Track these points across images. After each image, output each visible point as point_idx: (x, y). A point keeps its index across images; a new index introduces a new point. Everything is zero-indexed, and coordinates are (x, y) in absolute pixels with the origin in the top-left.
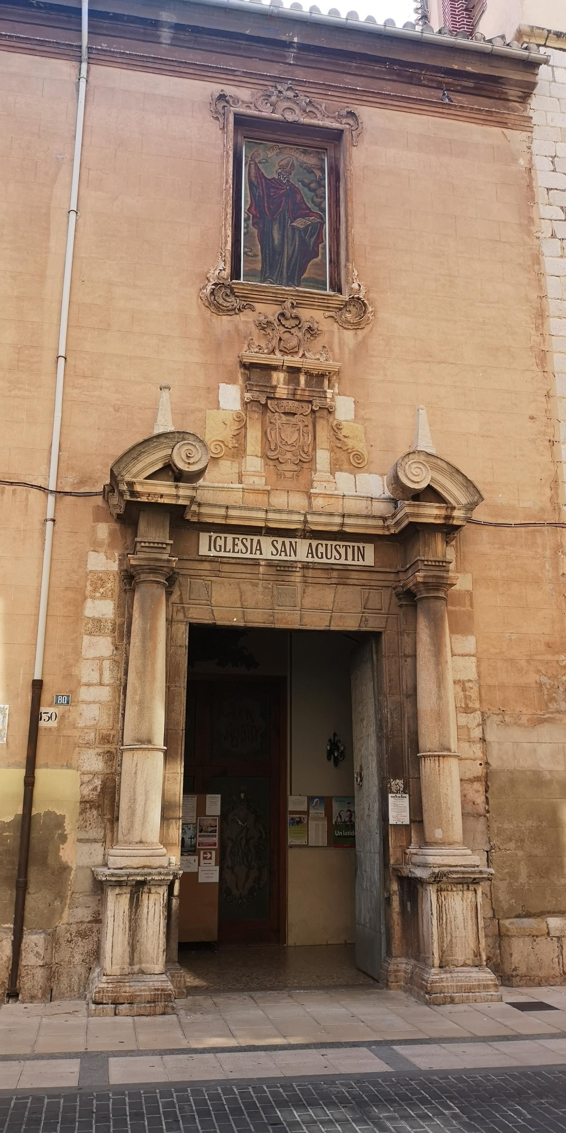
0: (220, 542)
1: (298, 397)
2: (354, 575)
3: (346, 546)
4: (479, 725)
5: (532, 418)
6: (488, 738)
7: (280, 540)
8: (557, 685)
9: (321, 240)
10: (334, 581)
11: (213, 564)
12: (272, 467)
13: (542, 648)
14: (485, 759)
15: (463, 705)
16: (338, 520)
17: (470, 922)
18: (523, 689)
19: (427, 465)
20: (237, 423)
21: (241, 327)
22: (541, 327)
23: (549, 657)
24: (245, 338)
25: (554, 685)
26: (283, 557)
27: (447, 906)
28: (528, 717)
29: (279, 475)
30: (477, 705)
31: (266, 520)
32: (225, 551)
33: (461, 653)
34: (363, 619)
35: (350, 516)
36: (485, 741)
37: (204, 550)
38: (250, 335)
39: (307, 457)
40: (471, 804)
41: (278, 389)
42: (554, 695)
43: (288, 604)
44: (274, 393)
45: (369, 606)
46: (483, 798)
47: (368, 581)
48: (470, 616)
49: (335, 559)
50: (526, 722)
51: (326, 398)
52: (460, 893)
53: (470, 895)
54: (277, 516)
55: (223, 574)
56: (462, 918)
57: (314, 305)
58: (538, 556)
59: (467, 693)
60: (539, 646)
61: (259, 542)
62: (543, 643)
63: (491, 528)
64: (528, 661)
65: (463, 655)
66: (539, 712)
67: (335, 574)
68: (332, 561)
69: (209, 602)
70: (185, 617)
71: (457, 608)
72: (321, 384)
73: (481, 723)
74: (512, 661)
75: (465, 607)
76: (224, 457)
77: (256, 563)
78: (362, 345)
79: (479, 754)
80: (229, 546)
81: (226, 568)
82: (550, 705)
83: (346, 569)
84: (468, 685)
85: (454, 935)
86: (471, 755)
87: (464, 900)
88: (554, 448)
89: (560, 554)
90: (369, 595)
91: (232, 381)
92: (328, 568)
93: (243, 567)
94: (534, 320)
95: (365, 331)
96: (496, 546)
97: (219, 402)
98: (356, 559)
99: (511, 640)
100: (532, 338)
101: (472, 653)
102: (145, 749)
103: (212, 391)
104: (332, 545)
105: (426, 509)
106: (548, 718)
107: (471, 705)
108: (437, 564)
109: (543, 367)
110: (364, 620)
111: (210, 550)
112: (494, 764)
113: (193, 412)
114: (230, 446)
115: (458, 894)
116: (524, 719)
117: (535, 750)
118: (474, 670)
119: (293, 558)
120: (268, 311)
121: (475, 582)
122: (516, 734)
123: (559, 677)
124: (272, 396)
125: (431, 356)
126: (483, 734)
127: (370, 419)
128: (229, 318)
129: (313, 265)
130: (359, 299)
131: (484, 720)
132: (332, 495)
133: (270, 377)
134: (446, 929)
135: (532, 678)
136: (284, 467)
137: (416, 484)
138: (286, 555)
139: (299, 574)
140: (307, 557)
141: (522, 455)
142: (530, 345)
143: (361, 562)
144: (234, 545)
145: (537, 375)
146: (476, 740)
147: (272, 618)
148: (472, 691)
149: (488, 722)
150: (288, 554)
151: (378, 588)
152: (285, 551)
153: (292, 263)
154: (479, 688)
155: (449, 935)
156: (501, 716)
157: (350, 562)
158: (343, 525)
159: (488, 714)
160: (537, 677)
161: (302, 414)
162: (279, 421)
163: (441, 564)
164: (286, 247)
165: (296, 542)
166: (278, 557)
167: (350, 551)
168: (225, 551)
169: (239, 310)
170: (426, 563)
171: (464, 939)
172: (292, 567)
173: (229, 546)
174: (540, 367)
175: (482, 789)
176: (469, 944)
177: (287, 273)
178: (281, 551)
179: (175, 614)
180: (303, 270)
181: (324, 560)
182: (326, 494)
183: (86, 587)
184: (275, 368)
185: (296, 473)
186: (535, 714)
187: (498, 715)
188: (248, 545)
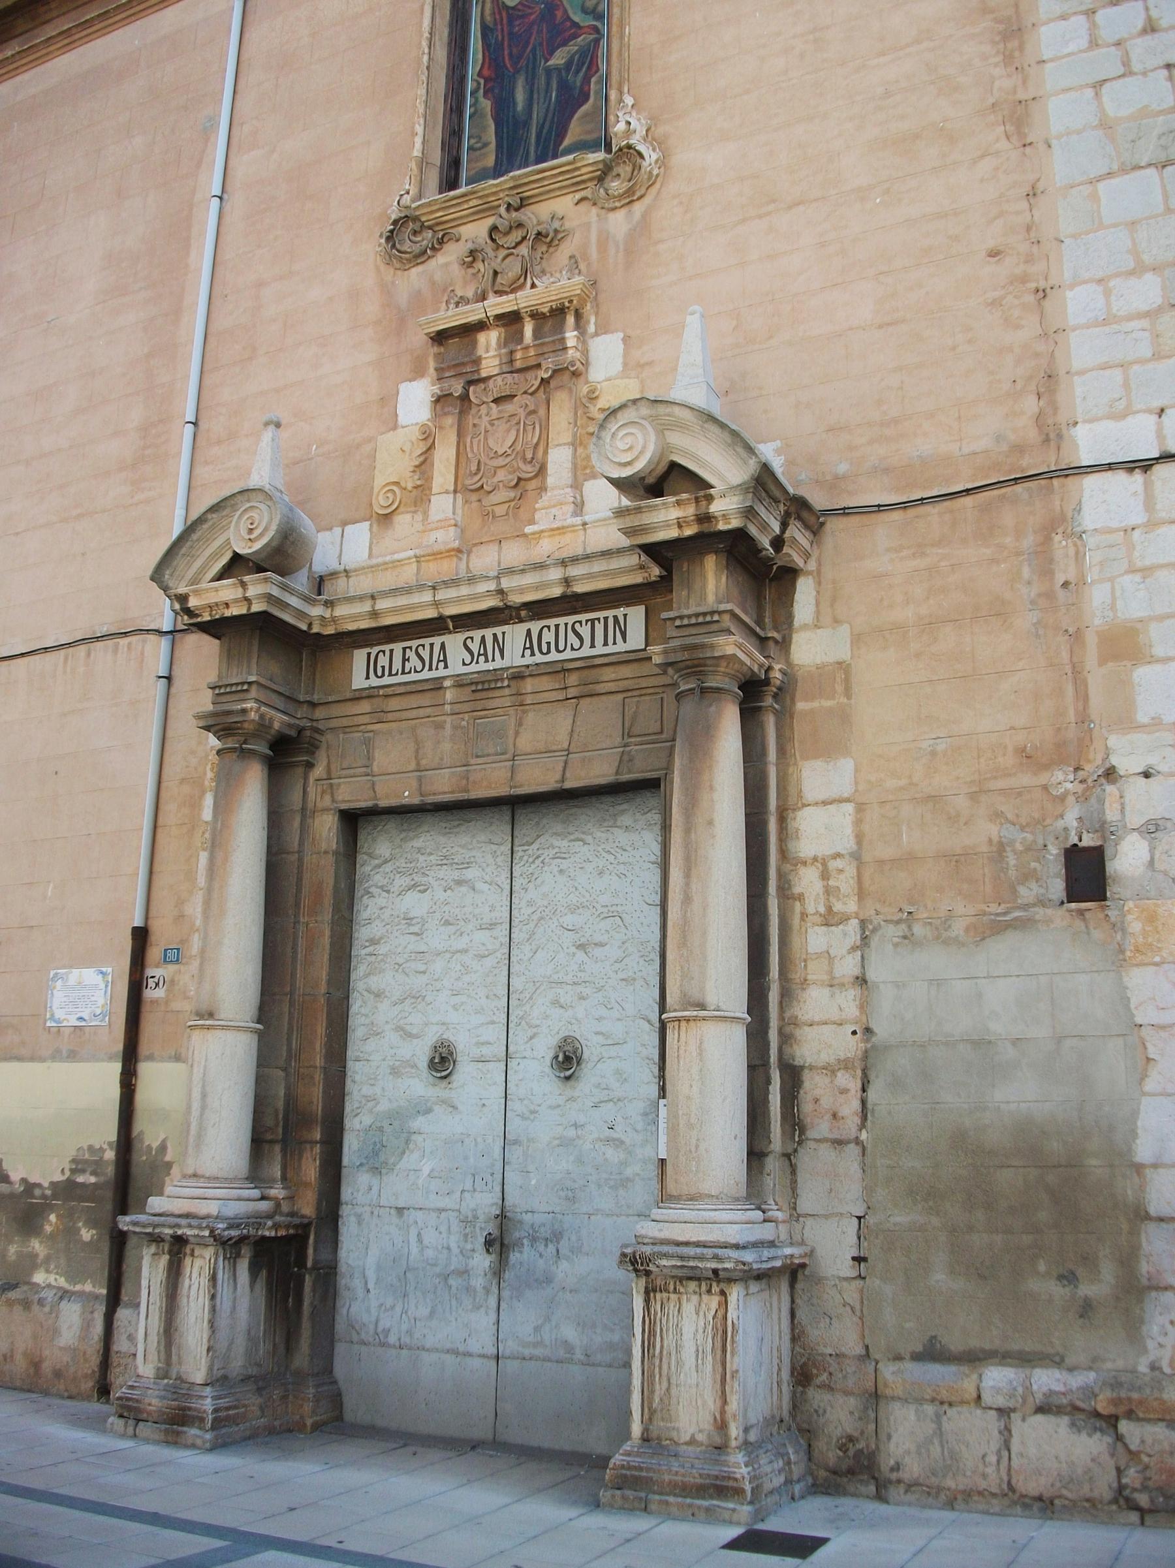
0: (383, 661)
1: (518, 364)
2: (609, 674)
3: (593, 621)
4: (854, 949)
5: (994, 254)
6: (871, 975)
7: (477, 634)
8: (1041, 842)
9: (594, 69)
10: (572, 692)
11: (375, 701)
12: (475, 505)
13: (1008, 760)
14: (864, 1020)
15: (822, 910)
16: (555, 574)
17: (710, 1358)
18: (957, 860)
19: (643, 422)
20: (421, 443)
21: (438, 277)
22: (1017, 54)
23: (1025, 779)
24: (444, 290)
25: (1034, 841)
26: (483, 666)
27: (664, 1322)
28: (969, 920)
29: (488, 515)
30: (852, 906)
31: (436, 604)
32: (390, 675)
33: (821, 797)
34: (626, 758)
35: (575, 560)
36: (865, 981)
37: (359, 681)
38: (451, 285)
39: (530, 469)
40: (828, 1117)
41: (484, 362)
42: (1033, 865)
43: (492, 751)
44: (478, 371)
45: (637, 730)
46: (856, 1105)
47: (636, 681)
48: (844, 717)
49: (573, 649)
50: (962, 933)
51: (566, 348)
52: (695, 1298)
53: (714, 1302)
54: (451, 593)
55: (390, 716)
56: (693, 1349)
57: (554, 190)
58: (1005, 554)
59: (831, 883)
60: (1000, 759)
61: (443, 646)
62: (1010, 749)
63: (896, 515)
64: (973, 797)
65: (825, 803)
66: (994, 908)
67: (573, 679)
68: (568, 654)
69: (369, 770)
70: (333, 801)
71: (816, 704)
72: (560, 327)
73: (858, 943)
74: (933, 799)
75: (833, 698)
76: (402, 509)
77: (436, 686)
78: (643, 227)
79: (851, 1010)
80: (397, 665)
81: (394, 704)
82: (1022, 890)
83: (590, 665)
84: (833, 865)
85: (673, 1381)
86: (835, 1015)
87: (701, 1314)
88: (1047, 303)
89: (1057, 538)
90: (637, 707)
91: (418, 372)
92: (559, 670)
93: (419, 695)
94: (1001, 46)
95: (647, 200)
96: (905, 553)
97: (396, 415)
98: (610, 640)
99: (933, 754)
100: (997, 84)
101: (846, 795)
102: (202, 1027)
103: (388, 401)
104: (566, 624)
105: (654, 513)
106: (1016, 919)
107: (838, 907)
108: (701, 620)
109: (1020, 134)
110: (625, 759)
111: (368, 678)
112: (883, 1031)
113: (358, 446)
114: (410, 486)
115: (688, 1300)
116: (958, 928)
117: (980, 995)
118: (849, 831)
119: (498, 663)
120: (476, 231)
121: (857, 640)
122: (937, 961)
123: (1048, 821)
124: (476, 377)
125: (774, 201)
126: (863, 967)
127: (650, 363)
128: (420, 268)
129: (578, 119)
130: (629, 147)
131: (865, 938)
132: (563, 528)
133: (474, 343)
134: (660, 1368)
135: (984, 832)
136: (495, 498)
137: (629, 468)
138: (487, 661)
139: (507, 692)
140: (523, 656)
141: (970, 341)
142: (991, 100)
143: (621, 647)
144: (405, 660)
145: (1008, 159)
146: (846, 980)
147: (464, 782)
148: (842, 877)
149: (875, 941)
150: (490, 658)
151: (657, 690)
152: (485, 654)
153: (545, 131)
154: (858, 869)
155: (665, 1379)
156: (903, 926)
157: (600, 650)
158: (567, 581)
159: (875, 922)
160: (993, 830)
161: (525, 393)
162: (488, 418)
163: (708, 618)
164: (535, 106)
165: (504, 633)
166: (474, 668)
167: (599, 628)
168: (390, 675)
169: (433, 248)
170: (678, 623)
171: (694, 1390)
172: (496, 681)
173: (397, 665)
174: (1014, 139)
175: (855, 1085)
176: (704, 1403)
177: (536, 152)
178: (479, 655)
179: (319, 799)
180: (561, 136)
181: (554, 656)
182: (552, 530)
183: (205, 774)
184: (481, 326)
185: (513, 504)
186: (985, 914)
187: (898, 922)
188: (426, 655)
